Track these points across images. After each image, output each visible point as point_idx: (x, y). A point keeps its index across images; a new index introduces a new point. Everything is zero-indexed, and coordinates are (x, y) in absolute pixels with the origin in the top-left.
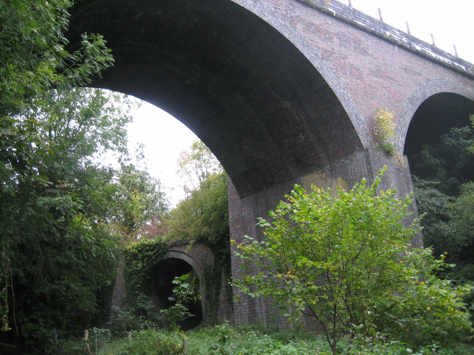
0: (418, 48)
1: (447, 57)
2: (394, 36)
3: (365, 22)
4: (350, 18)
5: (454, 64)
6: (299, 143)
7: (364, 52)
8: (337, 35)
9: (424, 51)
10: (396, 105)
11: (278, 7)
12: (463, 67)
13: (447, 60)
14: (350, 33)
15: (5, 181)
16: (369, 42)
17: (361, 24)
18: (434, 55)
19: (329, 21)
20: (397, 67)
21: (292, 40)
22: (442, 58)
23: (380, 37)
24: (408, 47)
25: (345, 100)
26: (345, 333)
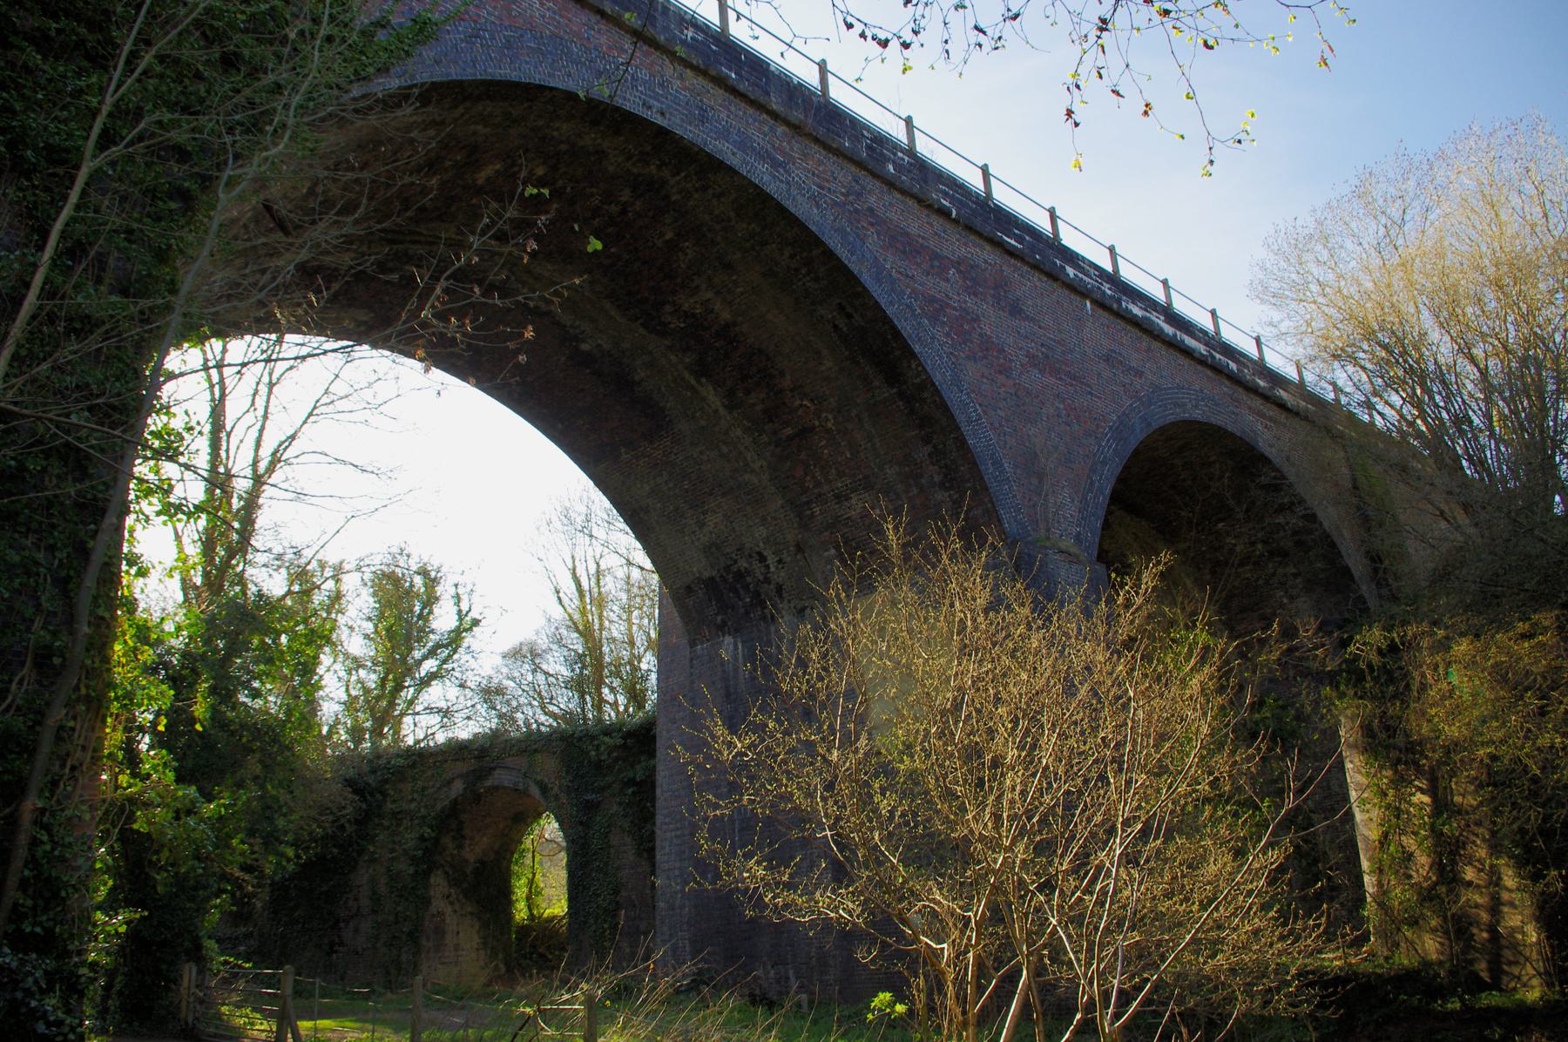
0: (1137, 311)
1: (1193, 336)
2: (1085, 278)
3: (1020, 239)
4: (988, 228)
5: (1213, 357)
6: (849, 518)
7: (1016, 310)
8: (958, 264)
9: (1149, 319)
10: (1084, 441)
11: (827, 185)
12: (1233, 366)
13: (1202, 349)
14: (986, 262)
15: (528, 341)
16: (1028, 285)
17: (1013, 242)
18: (1169, 330)
19: (265, 398)
20: (1089, 351)
21: (854, 268)
22: (1190, 342)
23: (1054, 276)
24: (1115, 306)
25: (969, 422)
26: (378, 22)
